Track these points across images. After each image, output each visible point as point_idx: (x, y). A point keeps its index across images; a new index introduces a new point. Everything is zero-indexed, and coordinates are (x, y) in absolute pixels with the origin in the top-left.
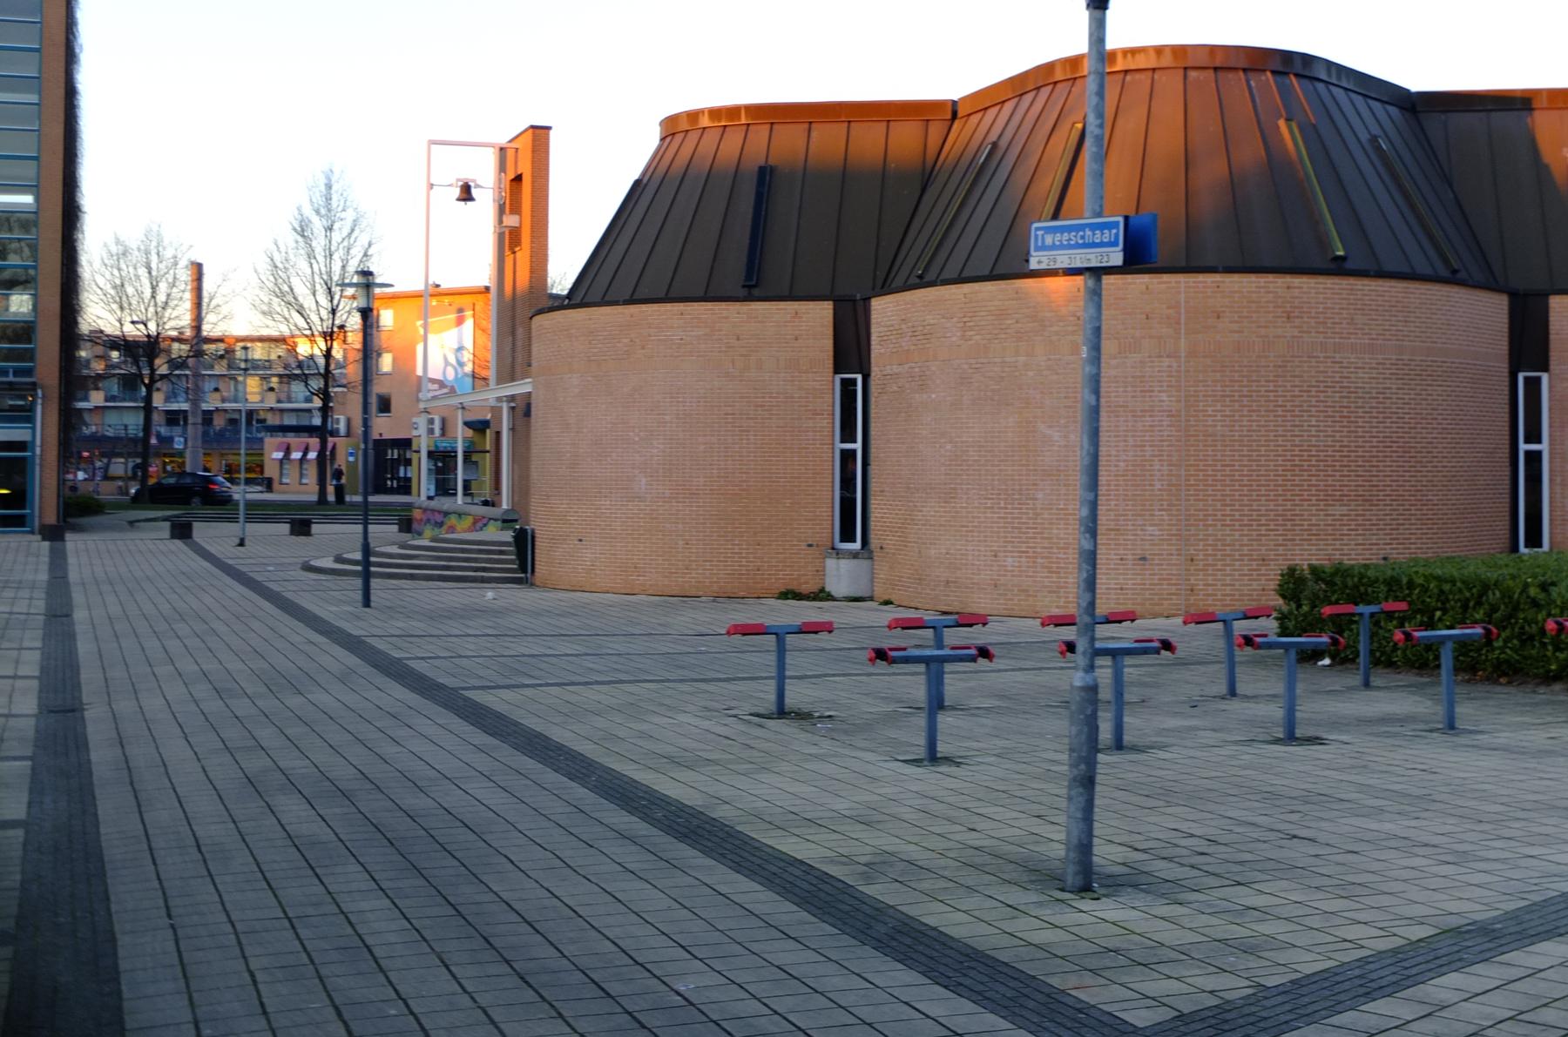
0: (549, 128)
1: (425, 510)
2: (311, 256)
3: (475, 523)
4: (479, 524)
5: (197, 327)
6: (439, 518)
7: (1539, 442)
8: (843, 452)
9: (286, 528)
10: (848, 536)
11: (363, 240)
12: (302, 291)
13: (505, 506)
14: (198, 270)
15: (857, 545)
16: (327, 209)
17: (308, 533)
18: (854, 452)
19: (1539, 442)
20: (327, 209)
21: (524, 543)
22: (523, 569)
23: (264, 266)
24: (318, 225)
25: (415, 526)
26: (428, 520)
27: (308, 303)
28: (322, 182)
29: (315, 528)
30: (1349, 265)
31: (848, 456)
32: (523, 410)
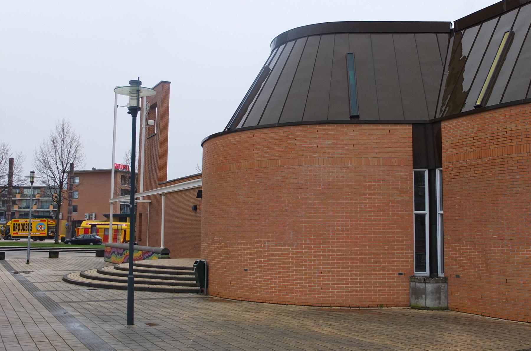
0: (170, 83)
1: (112, 247)
2: (56, 150)
3: (143, 254)
4: (145, 256)
5: (10, 181)
6: (121, 251)
7: (424, 210)
8: (417, 216)
9: (47, 254)
10: (420, 267)
11: (75, 145)
12: (52, 162)
13: (162, 247)
14: (11, 161)
15: (427, 273)
16: (63, 132)
17: (57, 257)
18: (424, 216)
19: (424, 210)
20: (63, 132)
21: (202, 269)
22: (202, 285)
23: (38, 151)
24: (59, 139)
25: (106, 254)
26: (114, 252)
27: (54, 168)
28: (61, 123)
29: (60, 255)
30: (362, 118)
31: (420, 220)
32: (68, 213)
